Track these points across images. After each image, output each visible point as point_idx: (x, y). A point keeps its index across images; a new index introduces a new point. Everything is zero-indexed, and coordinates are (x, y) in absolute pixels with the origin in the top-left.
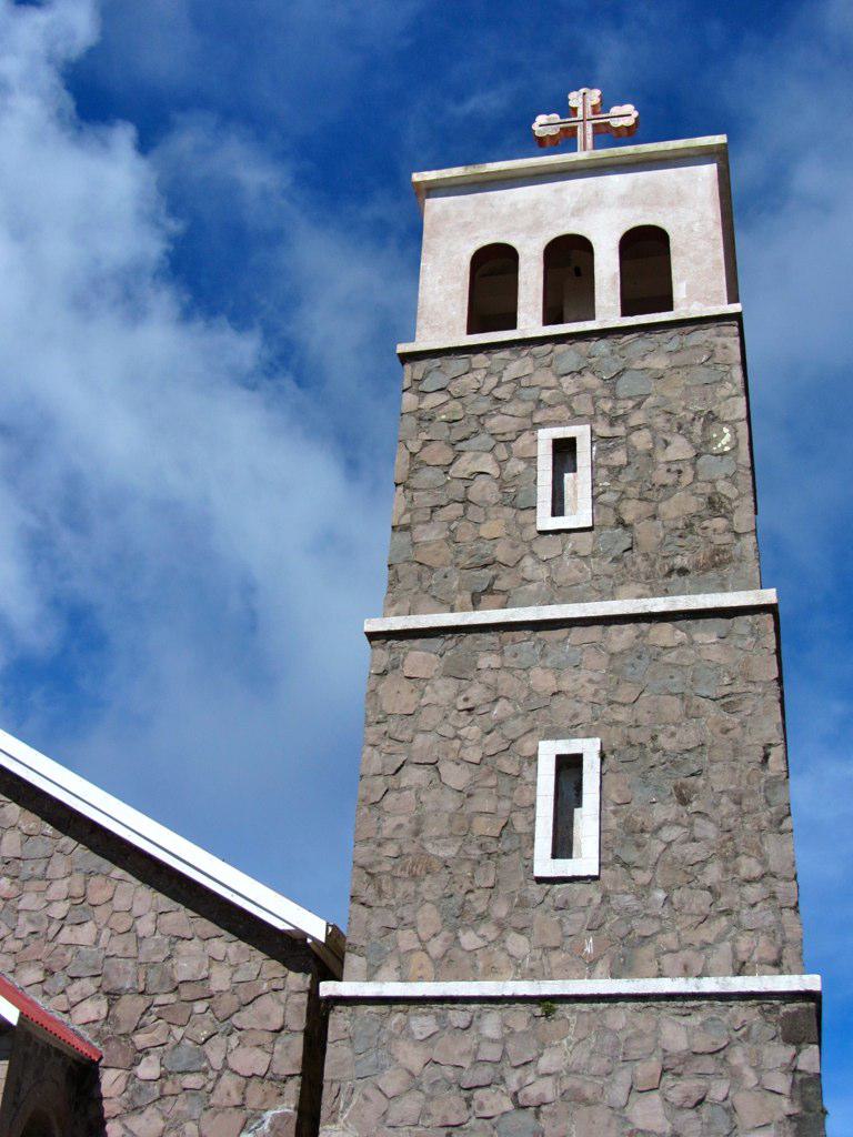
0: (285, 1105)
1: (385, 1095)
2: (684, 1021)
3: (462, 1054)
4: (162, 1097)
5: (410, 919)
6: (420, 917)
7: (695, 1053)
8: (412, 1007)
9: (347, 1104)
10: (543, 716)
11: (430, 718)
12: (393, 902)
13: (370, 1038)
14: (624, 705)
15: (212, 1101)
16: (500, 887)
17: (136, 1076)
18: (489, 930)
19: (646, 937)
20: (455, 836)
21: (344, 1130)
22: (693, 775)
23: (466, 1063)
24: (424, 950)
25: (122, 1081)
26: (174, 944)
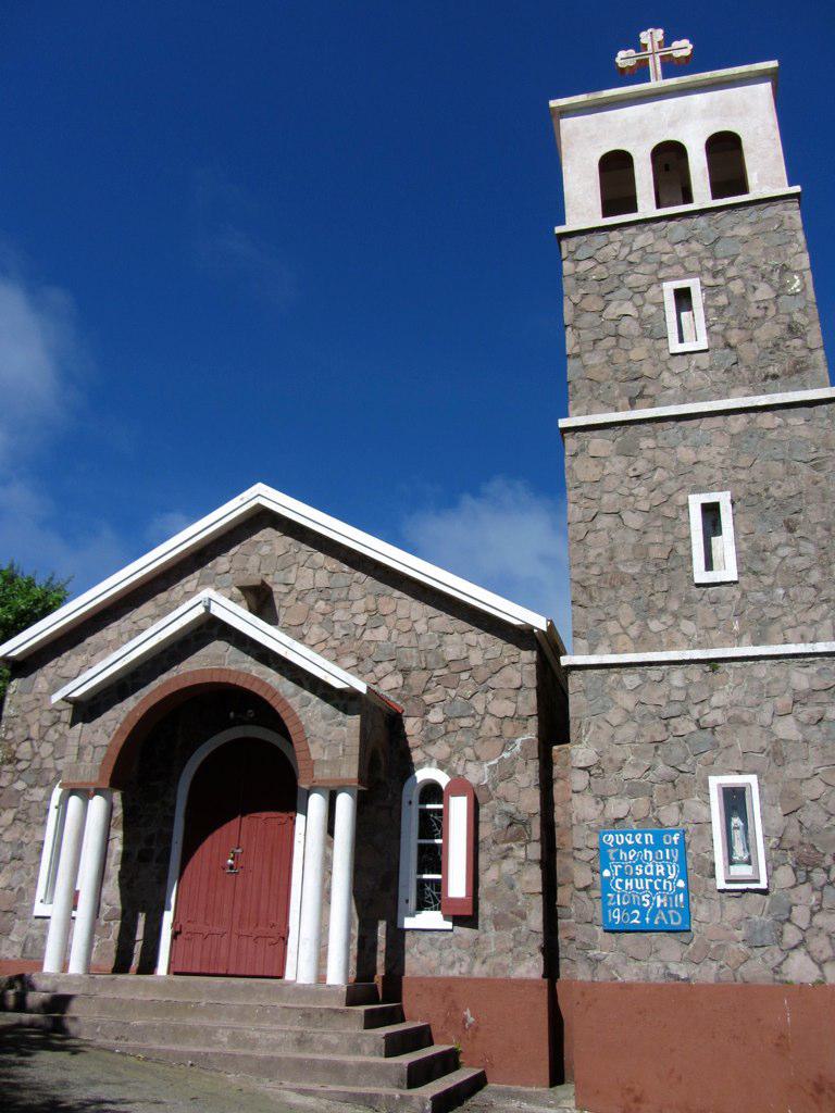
4: (447, 733)
11: (611, 483)
12: (601, 604)
14: (744, 468)
23: (663, 702)
24: (626, 633)
25: (419, 724)
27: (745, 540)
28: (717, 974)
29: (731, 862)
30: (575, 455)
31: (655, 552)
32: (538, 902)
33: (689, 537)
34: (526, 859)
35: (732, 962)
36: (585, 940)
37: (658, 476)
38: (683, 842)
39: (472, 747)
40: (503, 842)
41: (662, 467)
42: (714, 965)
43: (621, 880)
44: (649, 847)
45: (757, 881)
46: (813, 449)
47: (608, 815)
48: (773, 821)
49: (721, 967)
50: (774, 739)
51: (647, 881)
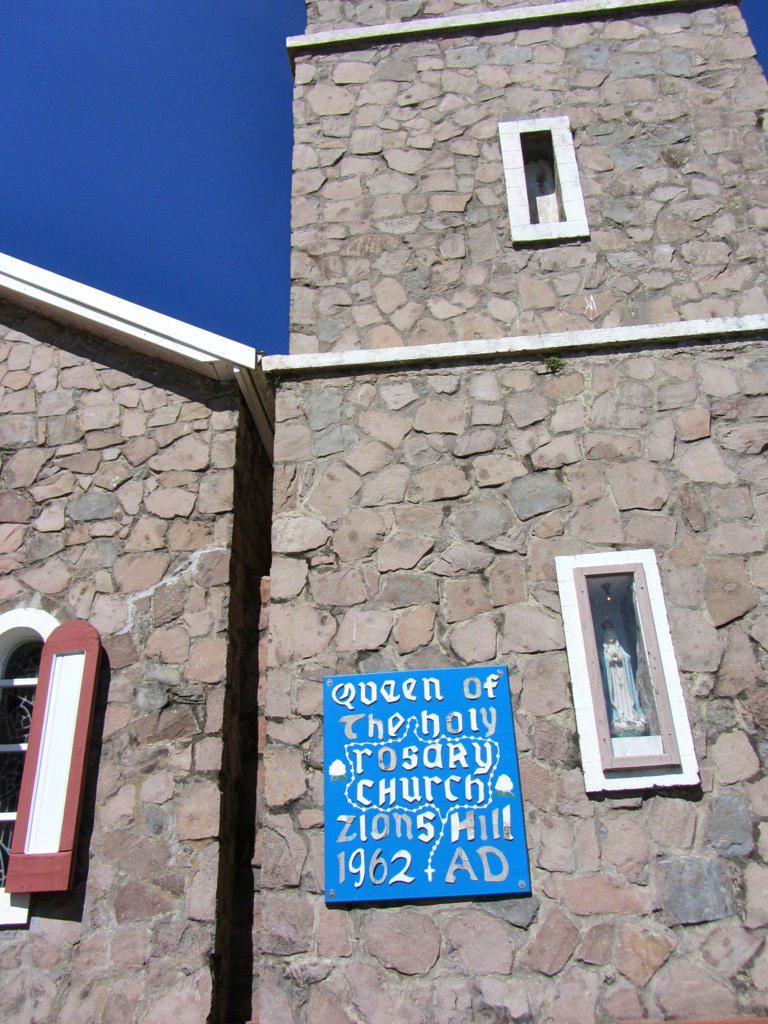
0: (216, 543)
1: (358, 473)
2: (726, 364)
3: (452, 420)
4: (67, 547)
5: (368, 294)
6: (378, 290)
7: (748, 396)
8: (382, 376)
9: (307, 486)
10: (495, 102)
11: (365, 117)
12: (344, 280)
13: (331, 412)
14: (589, 89)
15: (127, 547)
16: (472, 257)
17: (35, 529)
18: (467, 299)
19: (658, 290)
20: (412, 214)
21: (305, 515)
22: (680, 142)
23: (459, 428)
24: (389, 323)
25: (18, 536)
26: (80, 396)
27: (597, 180)
28: (599, 1001)
30: (312, 83)
31: (440, 203)
32: (209, 858)
33: (501, 180)
34: (192, 772)
35: (632, 966)
36: (284, 930)
37: (445, 104)
38: (503, 686)
40: (150, 740)
41: (452, 93)
42: (591, 976)
43: (369, 783)
44: (433, 706)
45: (676, 768)
46: (699, 61)
49: (609, 981)
50: (681, 482)
51: (428, 781)
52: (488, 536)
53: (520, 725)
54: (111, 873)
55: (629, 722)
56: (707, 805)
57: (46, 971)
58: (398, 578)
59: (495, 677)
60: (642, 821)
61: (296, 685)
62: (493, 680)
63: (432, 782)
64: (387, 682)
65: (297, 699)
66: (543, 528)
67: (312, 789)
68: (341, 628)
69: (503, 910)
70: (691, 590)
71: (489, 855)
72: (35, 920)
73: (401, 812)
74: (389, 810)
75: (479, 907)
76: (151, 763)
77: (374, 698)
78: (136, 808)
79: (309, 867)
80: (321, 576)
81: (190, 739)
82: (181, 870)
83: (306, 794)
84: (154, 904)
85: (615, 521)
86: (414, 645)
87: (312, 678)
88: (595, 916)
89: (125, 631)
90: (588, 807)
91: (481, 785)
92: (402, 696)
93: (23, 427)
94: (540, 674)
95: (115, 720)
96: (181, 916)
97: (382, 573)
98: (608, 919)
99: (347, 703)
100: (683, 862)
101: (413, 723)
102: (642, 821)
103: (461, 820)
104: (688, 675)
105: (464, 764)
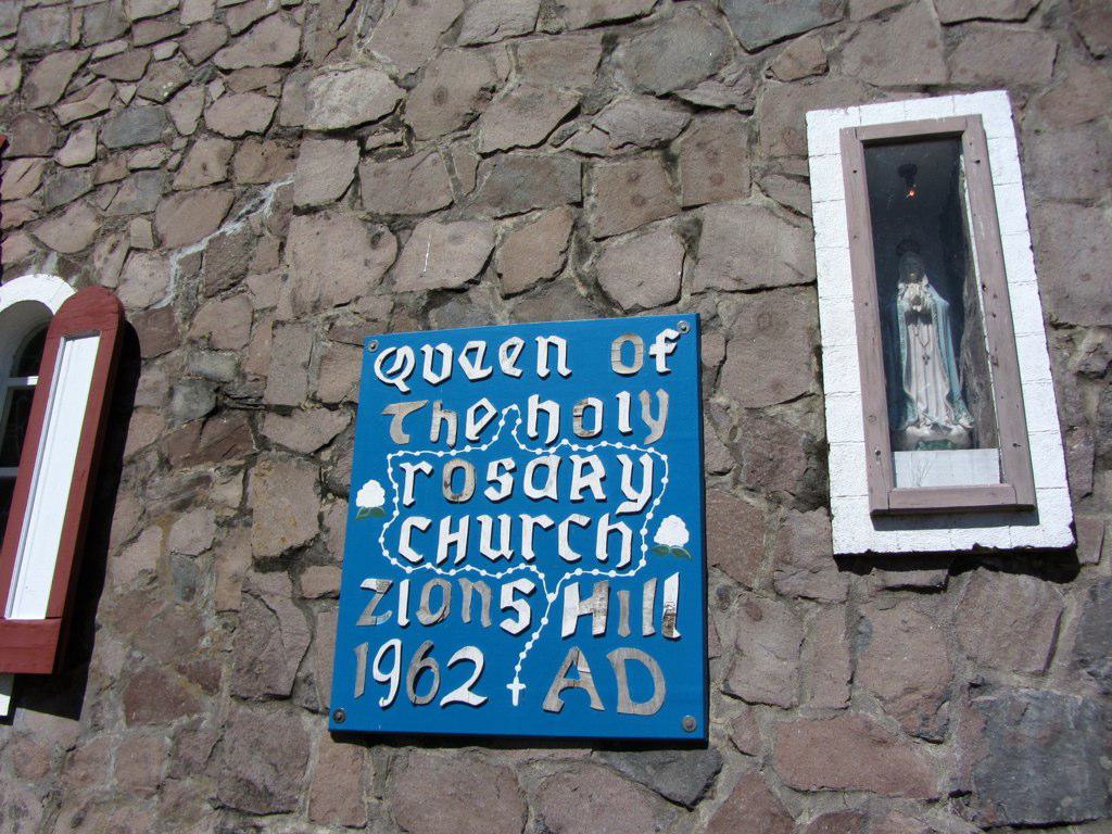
4: (97, 187)
15: (176, 183)
17: (57, 164)
25: (34, 176)
29: (898, 441)
36: (258, 772)
39: (149, 215)
40: (188, 462)
43: (422, 523)
44: (549, 386)
45: (1025, 514)
47: (407, 280)
48: (1085, 262)
51: (528, 522)
52: (681, 82)
53: (716, 425)
54: (122, 653)
55: (935, 426)
56: (1085, 590)
57: (31, 785)
58: (514, 162)
59: (672, 334)
60: (945, 615)
61: (319, 351)
62: (667, 340)
63: (536, 524)
64: (472, 344)
65: (319, 377)
66: (788, 64)
67: (328, 531)
68: (404, 253)
69: (649, 769)
70: (1080, 169)
71: (630, 663)
72: (21, 712)
73: (474, 576)
74: (453, 572)
75: (603, 760)
76: (184, 496)
77: (446, 372)
78: (161, 561)
79: (310, 666)
80: (380, 165)
81: (242, 462)
82: (217, 656)
83: (316, 539)
84: (177, 702)
85: (932, 45)
86: (530, 279)
87: (346, 339)
88: (828, 795)
89: (164, 303)
90: (835, 583)
91: (627, 533)
92: (497, 365)
93: (53, 23)
94: (761, 330)
95: (142, 433)
96: (213, 721)
97: (484, 156)
98: (855, 802)
99: (399, 381)
100: (1024, 700)
101: (512, 416)
102: (945, 615)
103: (582, 598)
104: (1063, 333)
105: (599, 494)
